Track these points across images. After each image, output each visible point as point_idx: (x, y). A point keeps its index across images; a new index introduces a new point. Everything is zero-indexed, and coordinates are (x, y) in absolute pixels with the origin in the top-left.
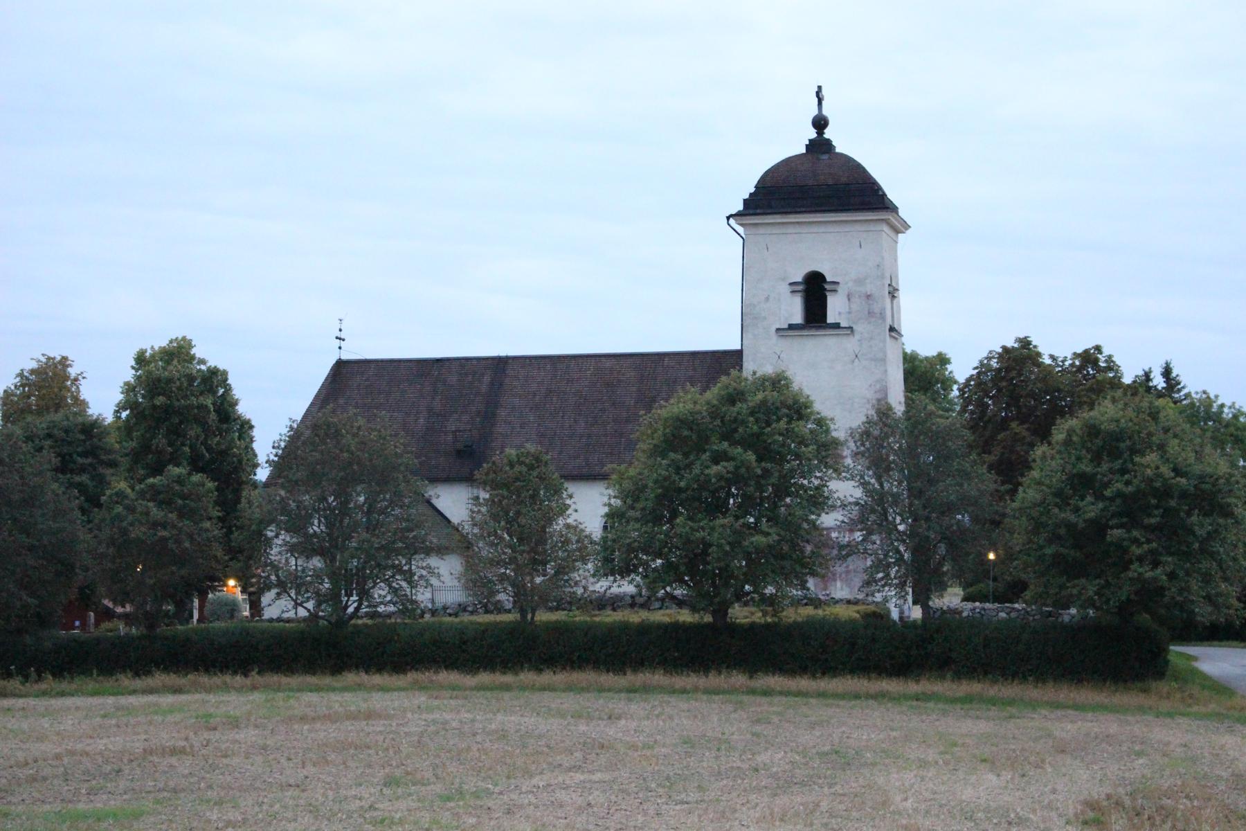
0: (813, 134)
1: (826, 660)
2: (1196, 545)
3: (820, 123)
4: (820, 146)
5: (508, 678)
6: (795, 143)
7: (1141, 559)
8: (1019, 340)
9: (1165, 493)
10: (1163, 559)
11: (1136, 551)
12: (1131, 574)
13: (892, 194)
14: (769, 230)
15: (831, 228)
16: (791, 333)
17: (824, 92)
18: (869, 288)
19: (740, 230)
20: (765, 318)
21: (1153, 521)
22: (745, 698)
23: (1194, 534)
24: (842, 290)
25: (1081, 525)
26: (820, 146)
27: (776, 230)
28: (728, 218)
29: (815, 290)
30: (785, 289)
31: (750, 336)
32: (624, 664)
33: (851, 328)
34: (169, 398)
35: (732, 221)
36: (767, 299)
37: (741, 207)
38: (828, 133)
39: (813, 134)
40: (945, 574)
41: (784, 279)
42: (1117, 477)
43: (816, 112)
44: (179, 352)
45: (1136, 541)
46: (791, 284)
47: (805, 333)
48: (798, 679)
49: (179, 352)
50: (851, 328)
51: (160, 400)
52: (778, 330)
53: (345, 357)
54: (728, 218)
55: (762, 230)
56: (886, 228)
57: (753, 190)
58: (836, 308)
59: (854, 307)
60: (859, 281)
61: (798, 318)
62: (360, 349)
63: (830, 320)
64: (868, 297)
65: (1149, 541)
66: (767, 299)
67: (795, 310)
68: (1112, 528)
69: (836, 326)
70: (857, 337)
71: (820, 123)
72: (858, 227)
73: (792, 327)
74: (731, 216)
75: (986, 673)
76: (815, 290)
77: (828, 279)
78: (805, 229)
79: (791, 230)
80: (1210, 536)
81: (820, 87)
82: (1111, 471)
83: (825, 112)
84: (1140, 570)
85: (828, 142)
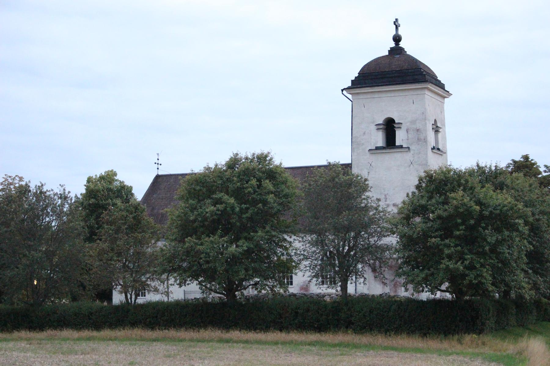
0: (393, 44)
1: (282, 322)
2: (487, 248)
3: (397, 39)
4: (397, 51)
5: (95, 333)
6: (383, 48)
7: (450, 257)
8: (523, 157)
9: (467, 214)
10: (466, 257)
11: (447, 251)
12: (442, 266)
13: (440, 77)
14: (365, 96)
15: (397, 94)
16: (378, 151)
17: (399, 22)
18: (419, 125)
19: (350, 96)
20: (363, 144)
21: (458, 233)
22: (218, 345)
23: (485, 240)
24: (404, 127)
25: (415, 236)
26: (397, 51)
27: (369, 96)
28: (342, 90)
29: (390, 127)
30: (374, 128)
31: (355, 154)
32: (347, 327)
33: (409, 148)
34: (97, 200)
35: (344, 92)
36: (364, 133)
37: (350, 85)
38: (402, 44)
39: (393, 44)
40: (338, 267)
41: (373, 123)
42: (441, 206)
43: (394, 33)
44: (109, 177)
45: (449, 246)
46: (376, 125)
47: (384, 151)
48: (202, 331)
49: (109, 177)
50: (409, 148)
51: (92, 201)
52: (370, 150)
53: (160, 173)
54: (342, 90)
55: (361, 96)
56: (427, 92)
57: (357, 75)
58: (400, 137)
59: (410, 136)
60: (413, 122)
61: (384, 145)
62: (170, 168)
63: (397, 143)
64: (418, 130)
65: (456, 246)
66: (364, 133)
67: (379, 139)
68: (431, 237)
69: (401, 147)
70: (412, 152)
71: (397, 39)
72: (412, 92)
73: (377, 148)
74: (344, 89)
75: (371, 330)
76: (390, 127)
77: (396, 122)
78: (383, 95)
79: (376, 95)
80: (499, 243)
81: (397, 20)
82: (438, 203)
83: (400, 32)
84: (447, 263)
85: (402, 49)
